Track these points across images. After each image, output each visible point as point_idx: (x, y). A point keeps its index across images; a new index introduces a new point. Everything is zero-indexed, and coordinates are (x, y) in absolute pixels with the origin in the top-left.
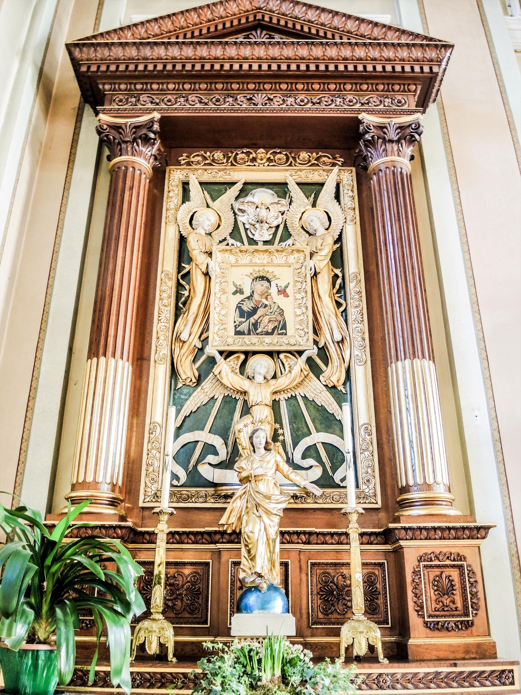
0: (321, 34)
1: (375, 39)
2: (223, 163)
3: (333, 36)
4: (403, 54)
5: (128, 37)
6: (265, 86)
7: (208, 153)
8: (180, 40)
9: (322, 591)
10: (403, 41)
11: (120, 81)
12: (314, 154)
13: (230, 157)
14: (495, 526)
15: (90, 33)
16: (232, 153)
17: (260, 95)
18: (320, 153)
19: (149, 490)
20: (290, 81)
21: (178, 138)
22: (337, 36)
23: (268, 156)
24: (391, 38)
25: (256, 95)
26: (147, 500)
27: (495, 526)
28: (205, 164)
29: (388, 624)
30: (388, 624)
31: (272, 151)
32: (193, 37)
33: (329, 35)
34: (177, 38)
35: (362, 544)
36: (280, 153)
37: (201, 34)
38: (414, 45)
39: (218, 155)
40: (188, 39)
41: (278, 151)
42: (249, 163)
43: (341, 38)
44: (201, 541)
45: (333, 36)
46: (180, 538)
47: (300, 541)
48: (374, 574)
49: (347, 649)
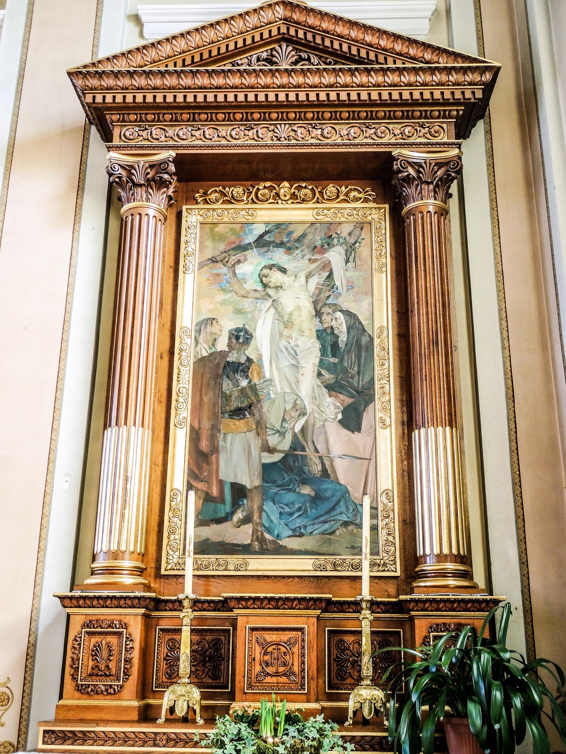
0: (372, 56)
1: (427, 62)
2: (243, 201)
3: (386, 59)
4: (330, 79)
5: (122, 65)
6: (166, 116)
7: (227, 189)
8: (178, 69)
9: (218, 660)
10: (408, 65)
11: (200, 111)
12: (343, 188)
13: (251, 192)
14: (54, 596)
15: (88, 61)
16: (254, 187)
17: (283, 125)
18: (349, 187)
19: (171, 557)
20: (138, 112)
21: (195, 174)
22: (390, 60)
23: (292, 190)
24: (443, 62)
25: (278, 126)
26: (169, 567)
27: (54, 596)
28: (224, 202)
29: (304, 689)
30: (304, 689)
31: (297, 185)
32: (184, 65)
33: (381, 59)
34: (167, 66)
35: (195, 610)
36: (306, 187)
37: (193, 62)
38: (453, 68)
39: (238, 190)
40: (188, 66)
41: (304, 185)
42: (271, 201)
43: (395, 62)
44: (268, 606)
45: (386, 59)
46: (246, 604)
47: (240, 606)
48: (219, 639)
49: (355, 713)
